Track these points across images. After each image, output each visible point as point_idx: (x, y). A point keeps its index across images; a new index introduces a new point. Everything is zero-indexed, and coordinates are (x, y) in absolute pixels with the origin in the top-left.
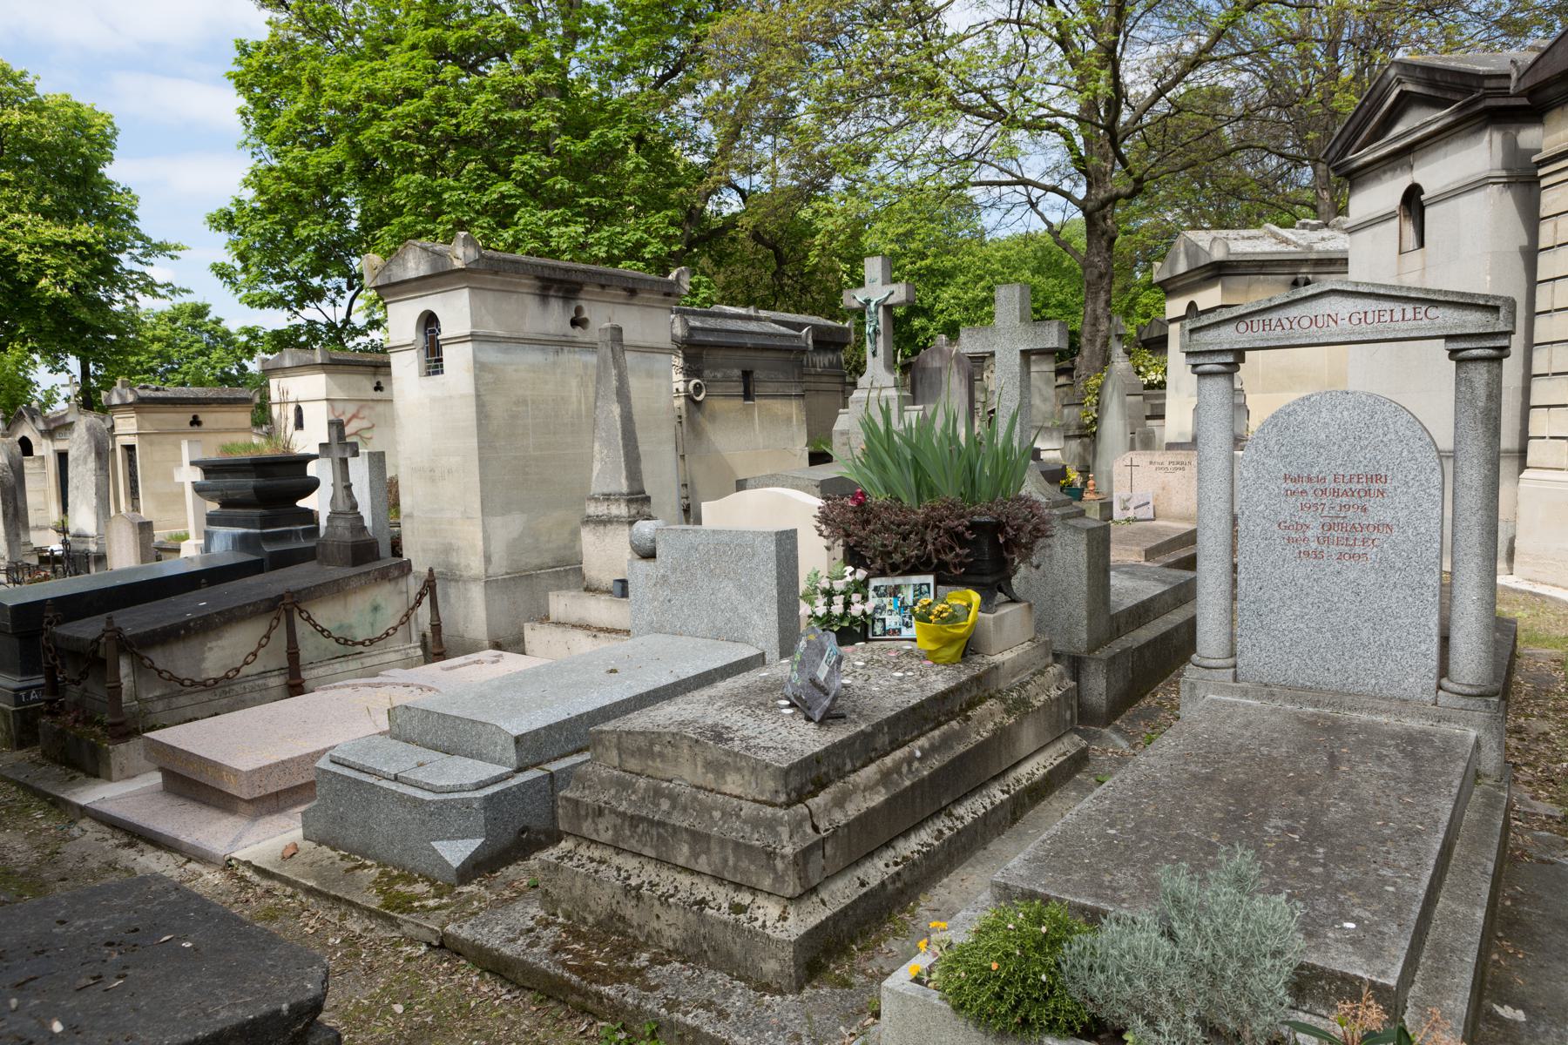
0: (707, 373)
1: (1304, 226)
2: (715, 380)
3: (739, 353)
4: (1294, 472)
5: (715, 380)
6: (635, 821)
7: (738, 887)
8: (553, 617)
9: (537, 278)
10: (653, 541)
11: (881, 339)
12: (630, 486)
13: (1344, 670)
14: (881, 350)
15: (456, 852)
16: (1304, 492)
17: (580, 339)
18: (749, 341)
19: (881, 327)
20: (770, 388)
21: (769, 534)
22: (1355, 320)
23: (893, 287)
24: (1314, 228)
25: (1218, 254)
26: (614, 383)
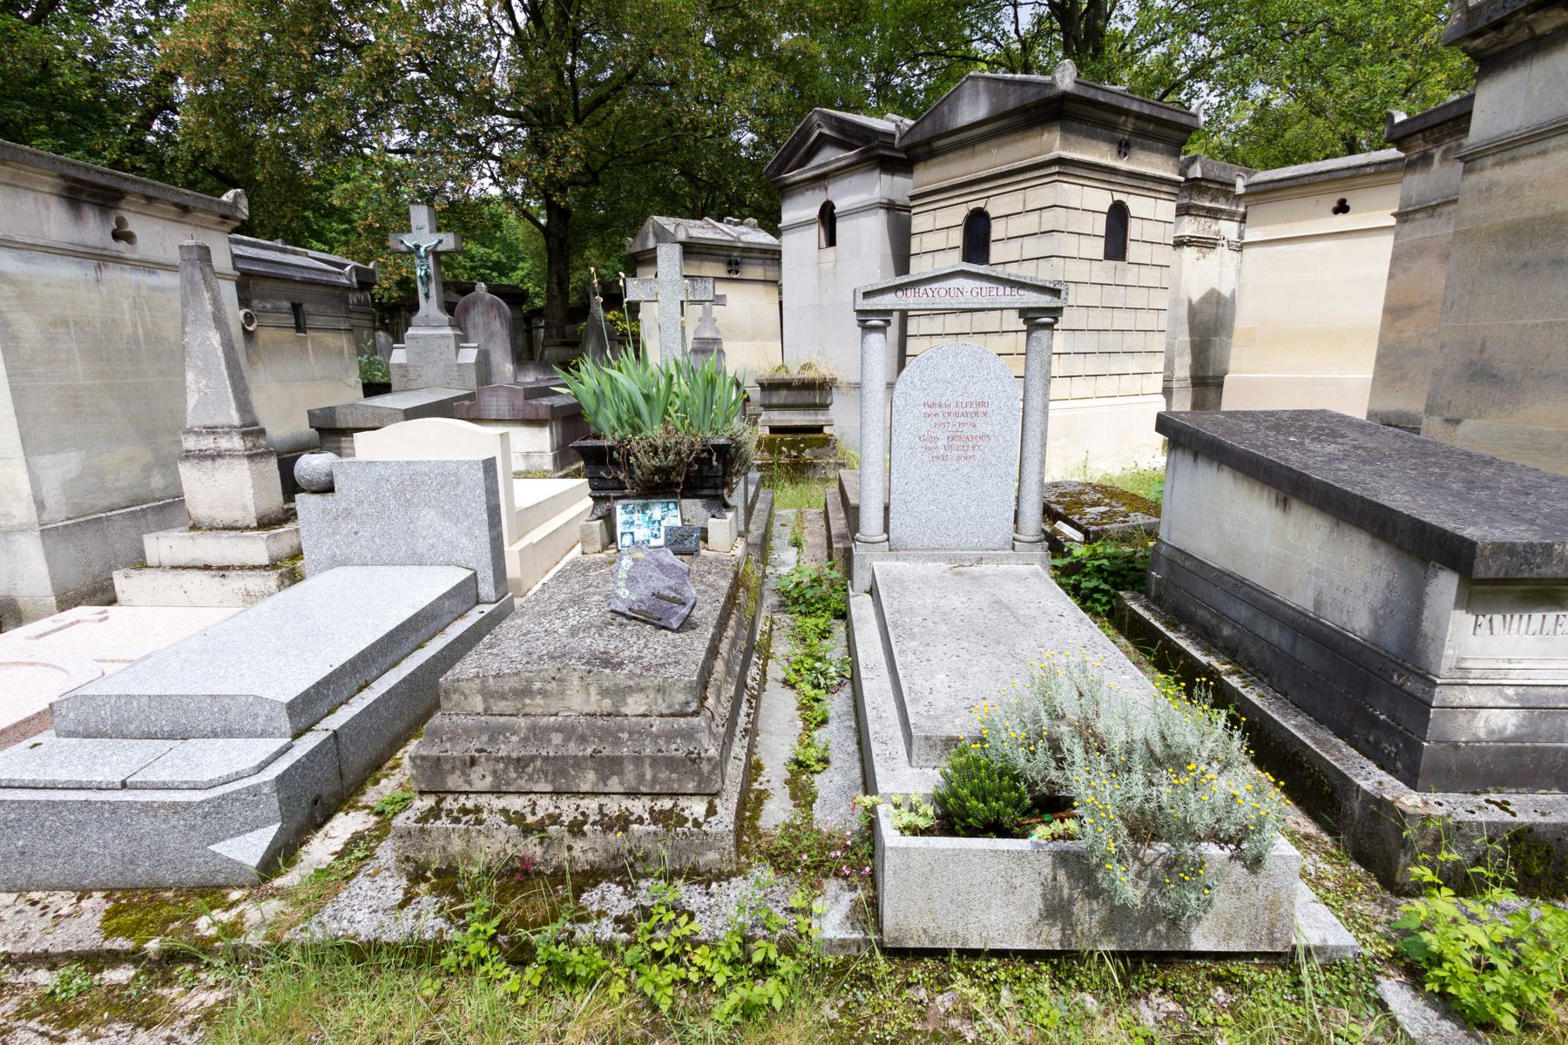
0: (255, 302)
1: (729, 222)
2: (264, 310)
4: (930, 400)
5: (264, 310)
6: (520, 763)
7: (655, 796)
8: (151, 559)
9: (62, 176)
10: (330, 475)
11: (433, 286)
12: (242, 417)
13: (959, 534)
15: (249, 849)
17: (128, 255)
18: (298, 275)
19: (431, 271)
20: (320, 321)
21: (476, 462)
23: (442, 236)
24: (736, 224)
26: (209, 308)
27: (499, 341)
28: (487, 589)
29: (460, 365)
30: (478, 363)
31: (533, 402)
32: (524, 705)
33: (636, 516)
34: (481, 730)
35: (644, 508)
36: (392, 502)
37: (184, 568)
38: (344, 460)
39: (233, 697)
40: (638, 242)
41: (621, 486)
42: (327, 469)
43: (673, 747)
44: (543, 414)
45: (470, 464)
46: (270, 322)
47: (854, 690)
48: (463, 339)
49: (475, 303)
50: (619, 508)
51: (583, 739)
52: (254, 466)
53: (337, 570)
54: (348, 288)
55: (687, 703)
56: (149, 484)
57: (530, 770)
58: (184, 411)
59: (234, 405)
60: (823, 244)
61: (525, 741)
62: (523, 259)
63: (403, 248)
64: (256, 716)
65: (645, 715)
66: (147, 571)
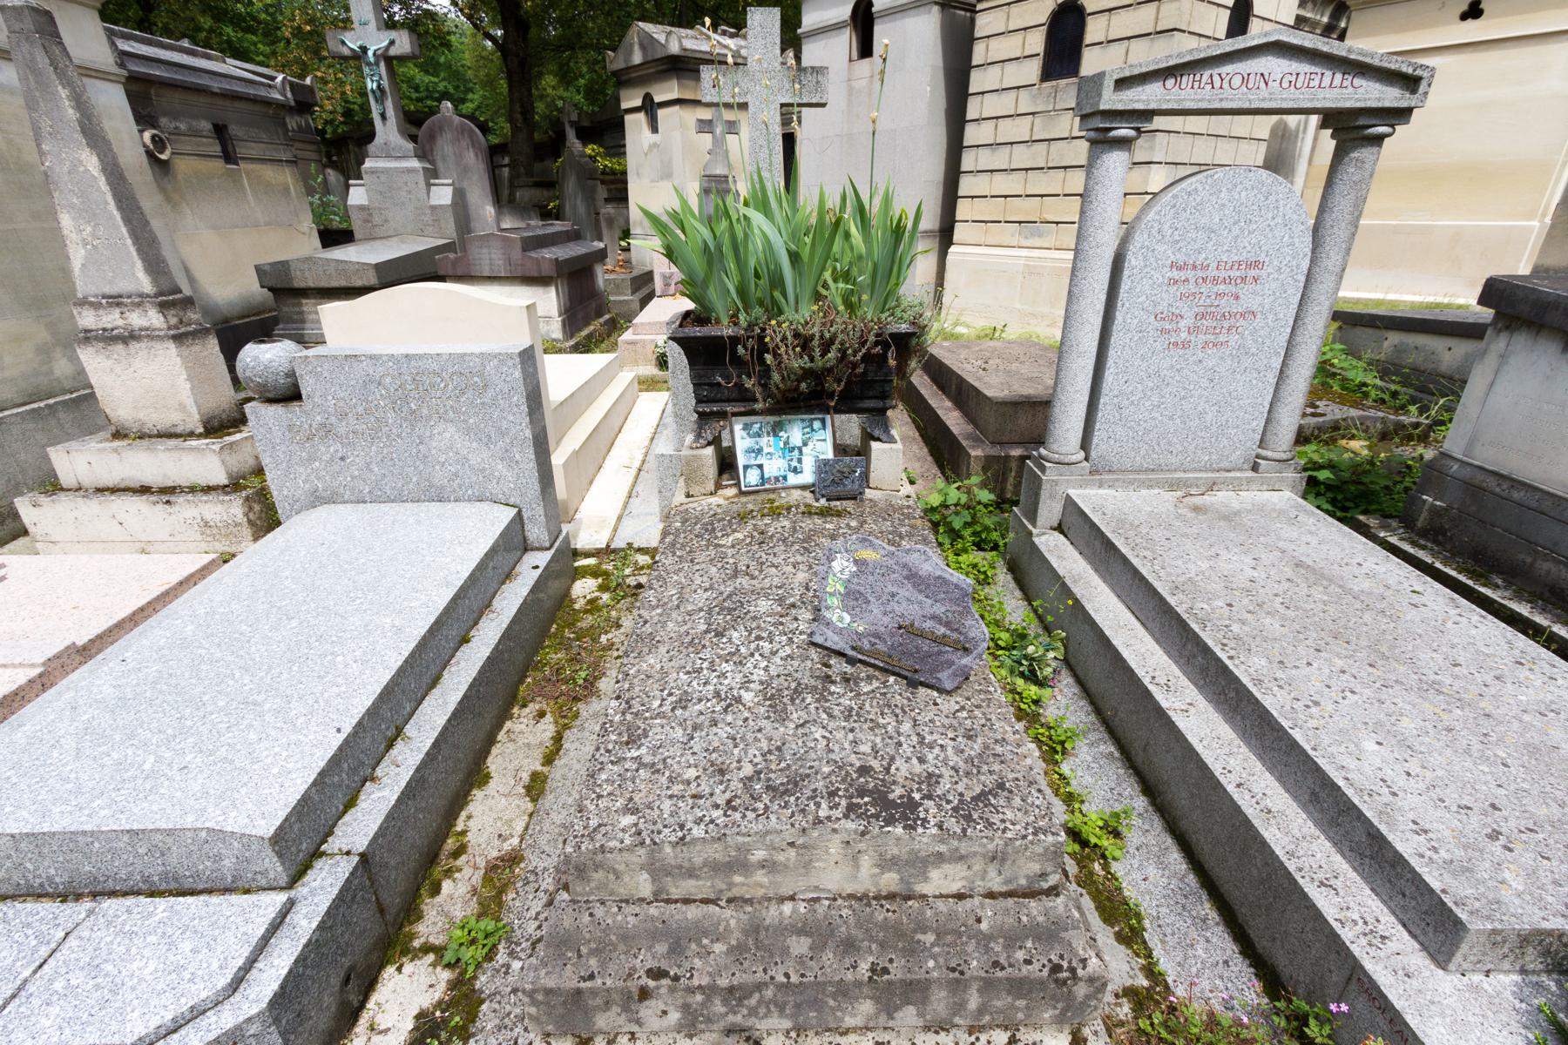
0: (163, 121)
1: (724, 33)
2: (177, 132)
3: (202, 99)
4: (1180, 258)
5: (177, 132)
10: (291, 374)
12: (155, 281)
14: (390, 113)
16: (1187, 280)
18: (215, 85)
19: (385, 83)
20: (254, 150)
21: (510, 356)
22: (1285, 85)
23: (393, 34)
24: (732, 36)
25: (674, 48)
26: (71, 114)
27: (475, 177)
28: (536, 532)
29: (433, 208)
30: (455, 204)
31: (533, 254)
32: (731, 885)
33: (764, 441)
34: (654, 934)
35: (776, 429)
36: (391, 415)
37: (114, 490)
38: (311, 352)
39: (170, 832)
40: (621, 57)
41: (745, 397)
42: (285, 367)
43: (1020, 955)
44: (547, 270)
45: (502, 358)
46: (188, 148)
47: (1079, 681)
48: (432, 174)
49: (441, 129)
50: (738, 428)
51: (849, 946)
52: (186, 352)
53: (322, 512)
54: (281, 106)
55: (1043, 875)
56: (51, 372)
57: (753, 1001)
58: (65, 271)
59: (139, 264)
60: (855, 55)
61: (738, 952)
62: (471, 90)
63: (346, 52)
64: (218, 858)
65: (960, 897)
66: (62, 495)
